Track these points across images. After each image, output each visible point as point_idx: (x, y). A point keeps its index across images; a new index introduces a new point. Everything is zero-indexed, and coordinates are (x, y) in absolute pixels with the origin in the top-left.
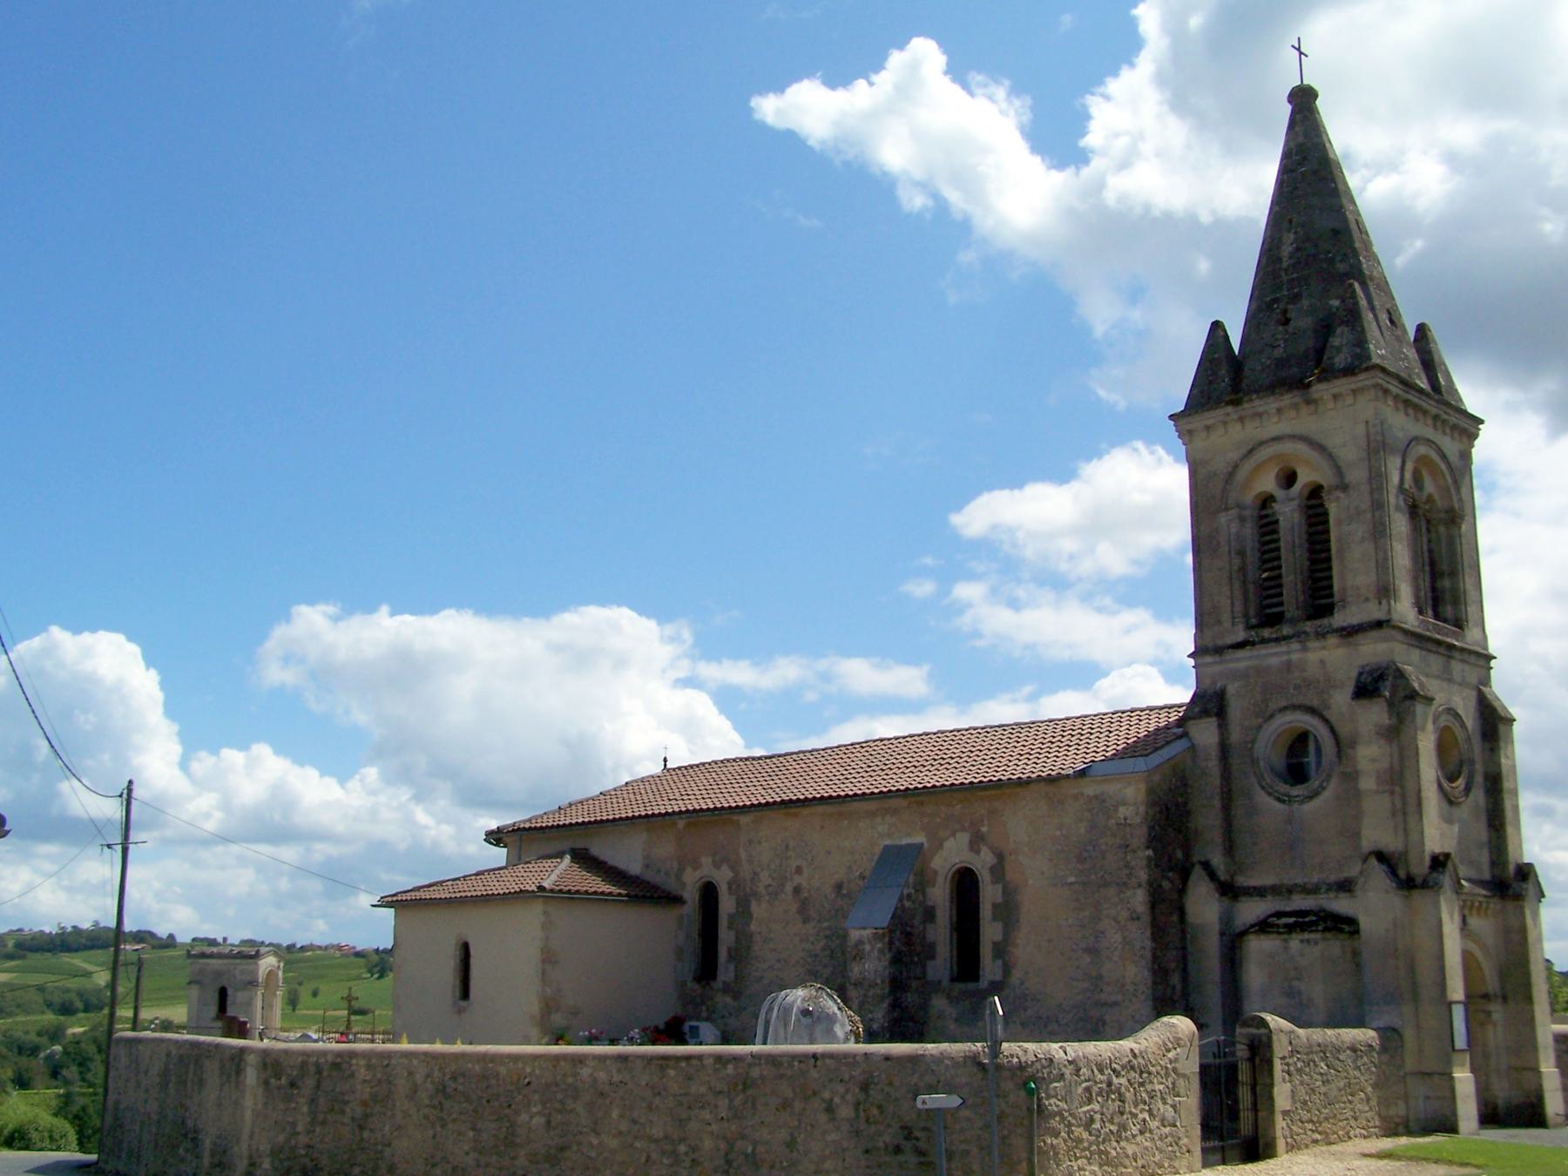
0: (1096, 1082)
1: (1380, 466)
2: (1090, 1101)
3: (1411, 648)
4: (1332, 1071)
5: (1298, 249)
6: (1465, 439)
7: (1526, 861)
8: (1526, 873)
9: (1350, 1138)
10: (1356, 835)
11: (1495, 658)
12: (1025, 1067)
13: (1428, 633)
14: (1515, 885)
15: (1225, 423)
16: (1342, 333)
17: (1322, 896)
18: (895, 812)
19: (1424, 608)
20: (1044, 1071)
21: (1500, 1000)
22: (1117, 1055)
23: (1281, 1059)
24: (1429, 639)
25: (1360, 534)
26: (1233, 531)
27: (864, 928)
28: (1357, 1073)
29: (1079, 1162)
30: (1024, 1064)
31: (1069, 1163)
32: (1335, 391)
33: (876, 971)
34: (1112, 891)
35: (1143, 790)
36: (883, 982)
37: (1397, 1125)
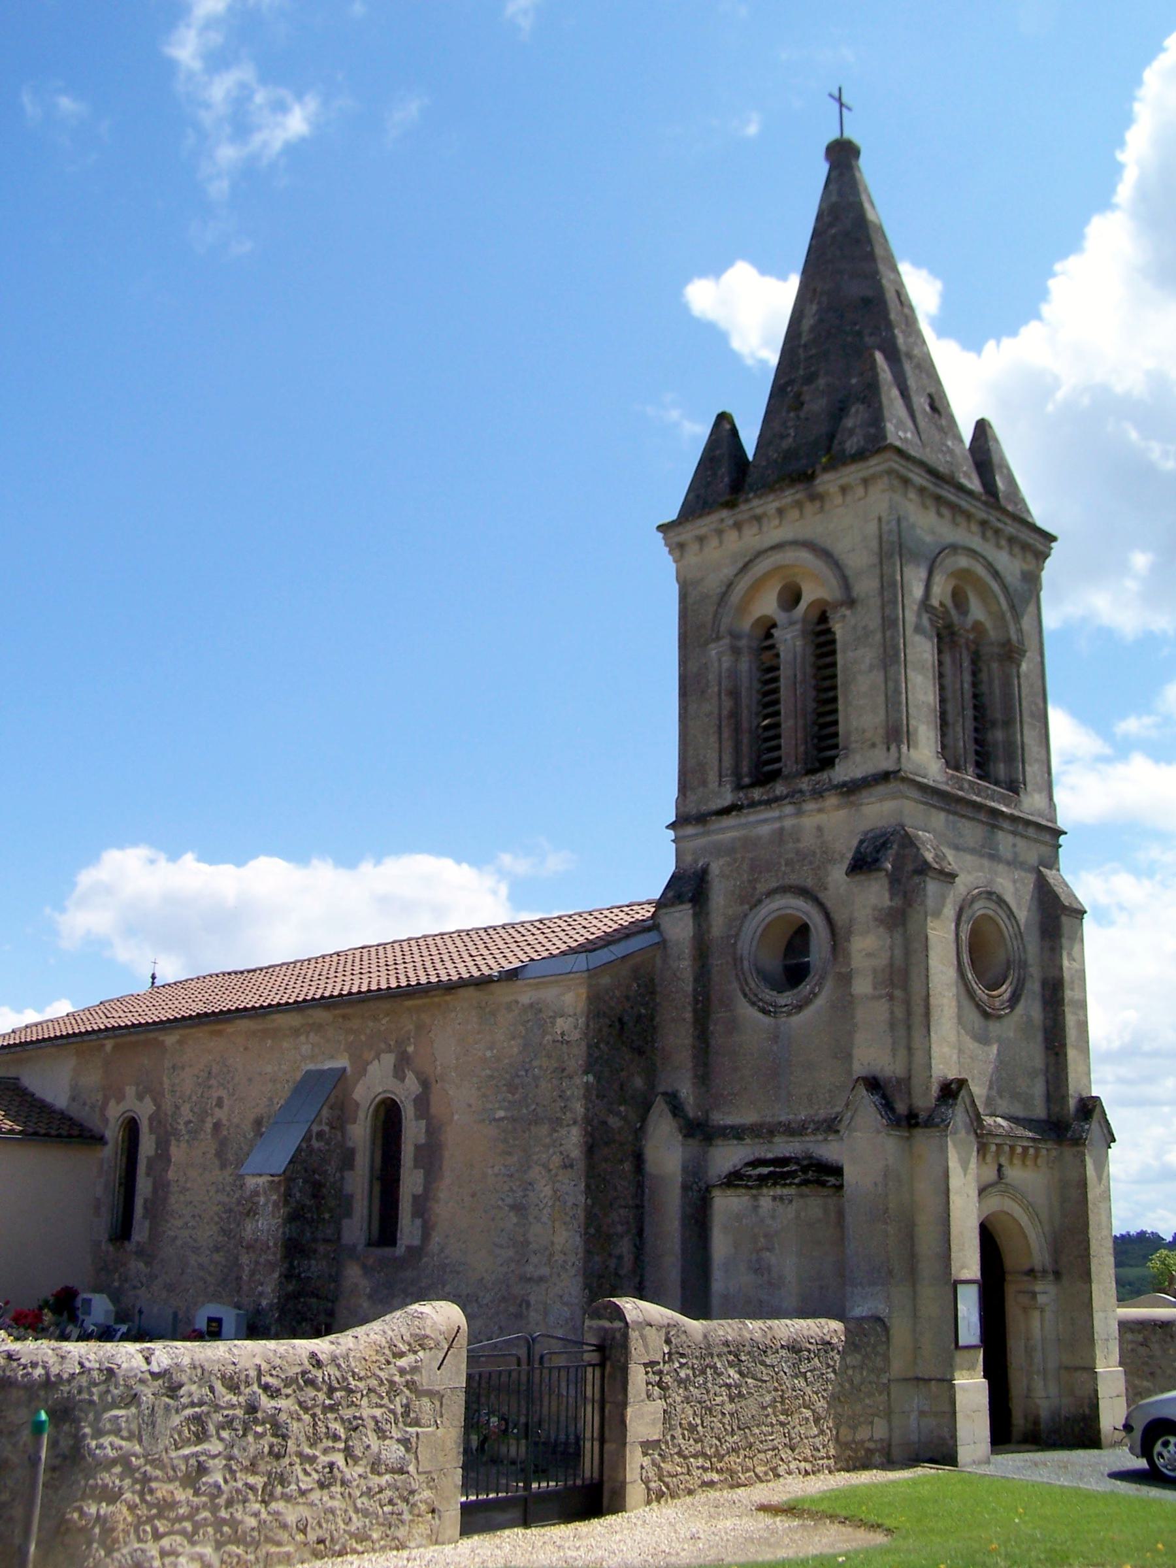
0: (217, 1408)
1: (894, 572)
2: (201, 1437)
3: (933, 810)
4: (749, 1381)
5: (821, 321)
6: (1030, 557)
7: (1093, 1095)
8: (1090, 1108)
9: (779, 1476)
10: (847, 1057)
11: (1066, 833)
12: (55, 1383)
13: (960, 793)
14: (1075, 1125)
15: (720, 532)
16: (857, 411)
17: (807, 1139)
18: (319, 1028)
19: (962, 763)
20: (94, 1390)
21: (1051, 1277)
22: (278, 1362)
23: (645, 1365)
24: (960, 800)
25: (867, 661)
26: (725, 665)
27: (260, 1175)
28: (800, 1383)
29: (165, 1542)
30: (53, 1379)
31: (136, 1545)
32: (843, 481)
33: (268, 1231)
34: (544, 1129)
35: (584, 996)
36: (275, 1244)
37: (870, 1451)
